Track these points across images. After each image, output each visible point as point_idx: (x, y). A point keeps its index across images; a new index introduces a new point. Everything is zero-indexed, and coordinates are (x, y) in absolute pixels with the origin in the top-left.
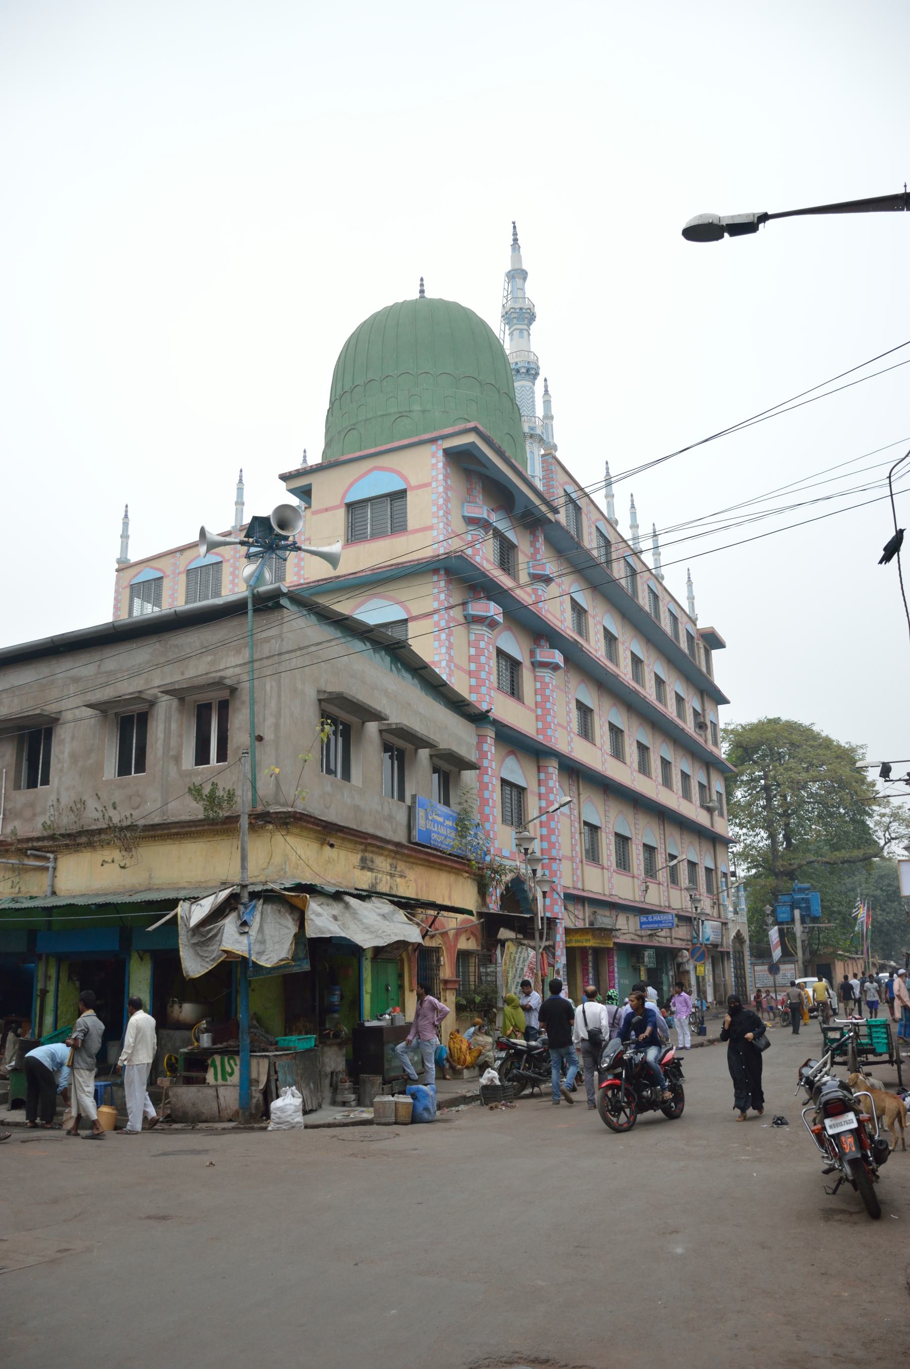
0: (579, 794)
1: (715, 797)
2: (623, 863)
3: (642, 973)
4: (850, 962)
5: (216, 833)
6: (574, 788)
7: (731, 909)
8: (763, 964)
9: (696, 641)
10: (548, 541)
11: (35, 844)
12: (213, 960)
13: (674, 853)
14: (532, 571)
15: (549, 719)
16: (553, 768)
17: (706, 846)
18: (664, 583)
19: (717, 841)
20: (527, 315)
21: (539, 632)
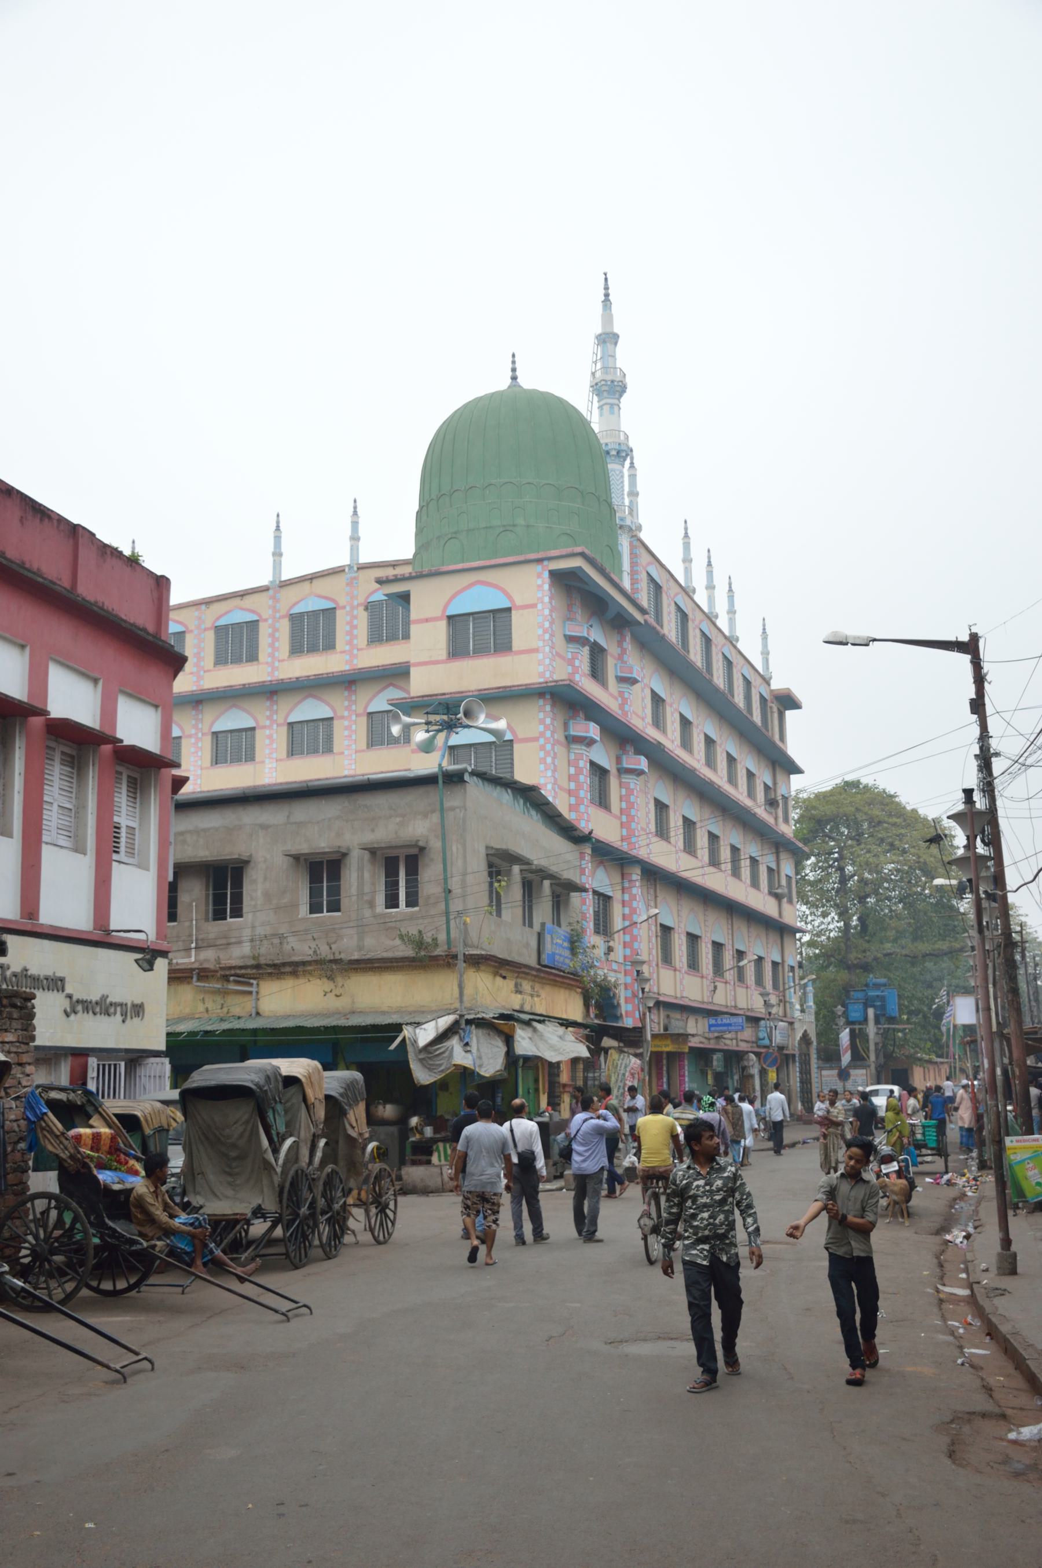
0: (656, 897)
1: (784, 882)
2: (693, 964)
3: (710, 1077)
4: (931, 1067)
5: (415, 968)
6: (652, 891)
7: (798, 1007)
8: (831, 1068)
9: (769, 704)
10: (635, 638)
11: (238, 972)
12: (442, 1071)
13: (742, 948)
14: (619, 674)
15: (633, 825)
16: (636, 874)
17: (774, 937)
18: (739, 645)
19: (783, 931)
20: (618, 389)
21: (622, 737)
